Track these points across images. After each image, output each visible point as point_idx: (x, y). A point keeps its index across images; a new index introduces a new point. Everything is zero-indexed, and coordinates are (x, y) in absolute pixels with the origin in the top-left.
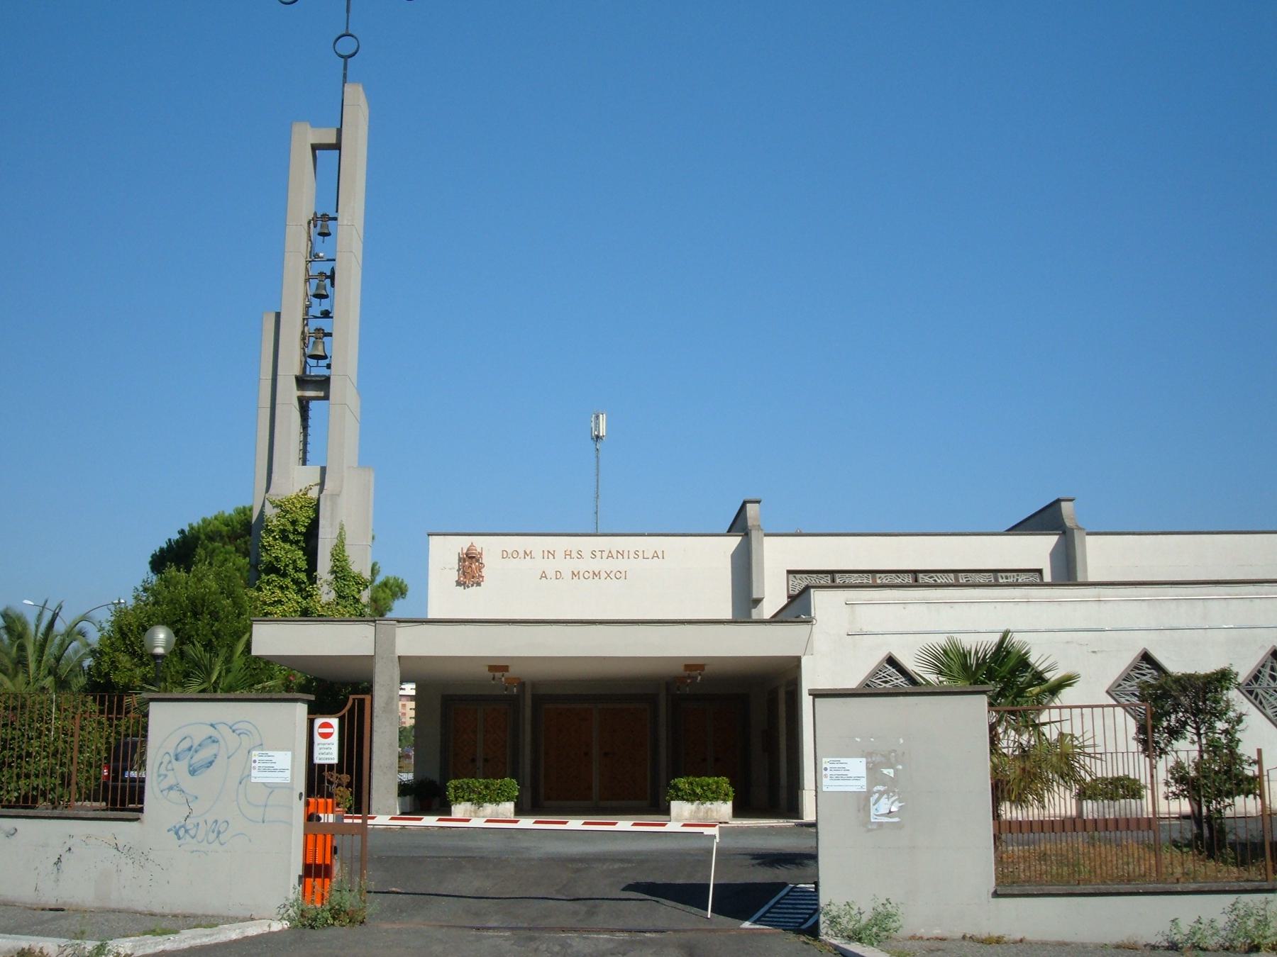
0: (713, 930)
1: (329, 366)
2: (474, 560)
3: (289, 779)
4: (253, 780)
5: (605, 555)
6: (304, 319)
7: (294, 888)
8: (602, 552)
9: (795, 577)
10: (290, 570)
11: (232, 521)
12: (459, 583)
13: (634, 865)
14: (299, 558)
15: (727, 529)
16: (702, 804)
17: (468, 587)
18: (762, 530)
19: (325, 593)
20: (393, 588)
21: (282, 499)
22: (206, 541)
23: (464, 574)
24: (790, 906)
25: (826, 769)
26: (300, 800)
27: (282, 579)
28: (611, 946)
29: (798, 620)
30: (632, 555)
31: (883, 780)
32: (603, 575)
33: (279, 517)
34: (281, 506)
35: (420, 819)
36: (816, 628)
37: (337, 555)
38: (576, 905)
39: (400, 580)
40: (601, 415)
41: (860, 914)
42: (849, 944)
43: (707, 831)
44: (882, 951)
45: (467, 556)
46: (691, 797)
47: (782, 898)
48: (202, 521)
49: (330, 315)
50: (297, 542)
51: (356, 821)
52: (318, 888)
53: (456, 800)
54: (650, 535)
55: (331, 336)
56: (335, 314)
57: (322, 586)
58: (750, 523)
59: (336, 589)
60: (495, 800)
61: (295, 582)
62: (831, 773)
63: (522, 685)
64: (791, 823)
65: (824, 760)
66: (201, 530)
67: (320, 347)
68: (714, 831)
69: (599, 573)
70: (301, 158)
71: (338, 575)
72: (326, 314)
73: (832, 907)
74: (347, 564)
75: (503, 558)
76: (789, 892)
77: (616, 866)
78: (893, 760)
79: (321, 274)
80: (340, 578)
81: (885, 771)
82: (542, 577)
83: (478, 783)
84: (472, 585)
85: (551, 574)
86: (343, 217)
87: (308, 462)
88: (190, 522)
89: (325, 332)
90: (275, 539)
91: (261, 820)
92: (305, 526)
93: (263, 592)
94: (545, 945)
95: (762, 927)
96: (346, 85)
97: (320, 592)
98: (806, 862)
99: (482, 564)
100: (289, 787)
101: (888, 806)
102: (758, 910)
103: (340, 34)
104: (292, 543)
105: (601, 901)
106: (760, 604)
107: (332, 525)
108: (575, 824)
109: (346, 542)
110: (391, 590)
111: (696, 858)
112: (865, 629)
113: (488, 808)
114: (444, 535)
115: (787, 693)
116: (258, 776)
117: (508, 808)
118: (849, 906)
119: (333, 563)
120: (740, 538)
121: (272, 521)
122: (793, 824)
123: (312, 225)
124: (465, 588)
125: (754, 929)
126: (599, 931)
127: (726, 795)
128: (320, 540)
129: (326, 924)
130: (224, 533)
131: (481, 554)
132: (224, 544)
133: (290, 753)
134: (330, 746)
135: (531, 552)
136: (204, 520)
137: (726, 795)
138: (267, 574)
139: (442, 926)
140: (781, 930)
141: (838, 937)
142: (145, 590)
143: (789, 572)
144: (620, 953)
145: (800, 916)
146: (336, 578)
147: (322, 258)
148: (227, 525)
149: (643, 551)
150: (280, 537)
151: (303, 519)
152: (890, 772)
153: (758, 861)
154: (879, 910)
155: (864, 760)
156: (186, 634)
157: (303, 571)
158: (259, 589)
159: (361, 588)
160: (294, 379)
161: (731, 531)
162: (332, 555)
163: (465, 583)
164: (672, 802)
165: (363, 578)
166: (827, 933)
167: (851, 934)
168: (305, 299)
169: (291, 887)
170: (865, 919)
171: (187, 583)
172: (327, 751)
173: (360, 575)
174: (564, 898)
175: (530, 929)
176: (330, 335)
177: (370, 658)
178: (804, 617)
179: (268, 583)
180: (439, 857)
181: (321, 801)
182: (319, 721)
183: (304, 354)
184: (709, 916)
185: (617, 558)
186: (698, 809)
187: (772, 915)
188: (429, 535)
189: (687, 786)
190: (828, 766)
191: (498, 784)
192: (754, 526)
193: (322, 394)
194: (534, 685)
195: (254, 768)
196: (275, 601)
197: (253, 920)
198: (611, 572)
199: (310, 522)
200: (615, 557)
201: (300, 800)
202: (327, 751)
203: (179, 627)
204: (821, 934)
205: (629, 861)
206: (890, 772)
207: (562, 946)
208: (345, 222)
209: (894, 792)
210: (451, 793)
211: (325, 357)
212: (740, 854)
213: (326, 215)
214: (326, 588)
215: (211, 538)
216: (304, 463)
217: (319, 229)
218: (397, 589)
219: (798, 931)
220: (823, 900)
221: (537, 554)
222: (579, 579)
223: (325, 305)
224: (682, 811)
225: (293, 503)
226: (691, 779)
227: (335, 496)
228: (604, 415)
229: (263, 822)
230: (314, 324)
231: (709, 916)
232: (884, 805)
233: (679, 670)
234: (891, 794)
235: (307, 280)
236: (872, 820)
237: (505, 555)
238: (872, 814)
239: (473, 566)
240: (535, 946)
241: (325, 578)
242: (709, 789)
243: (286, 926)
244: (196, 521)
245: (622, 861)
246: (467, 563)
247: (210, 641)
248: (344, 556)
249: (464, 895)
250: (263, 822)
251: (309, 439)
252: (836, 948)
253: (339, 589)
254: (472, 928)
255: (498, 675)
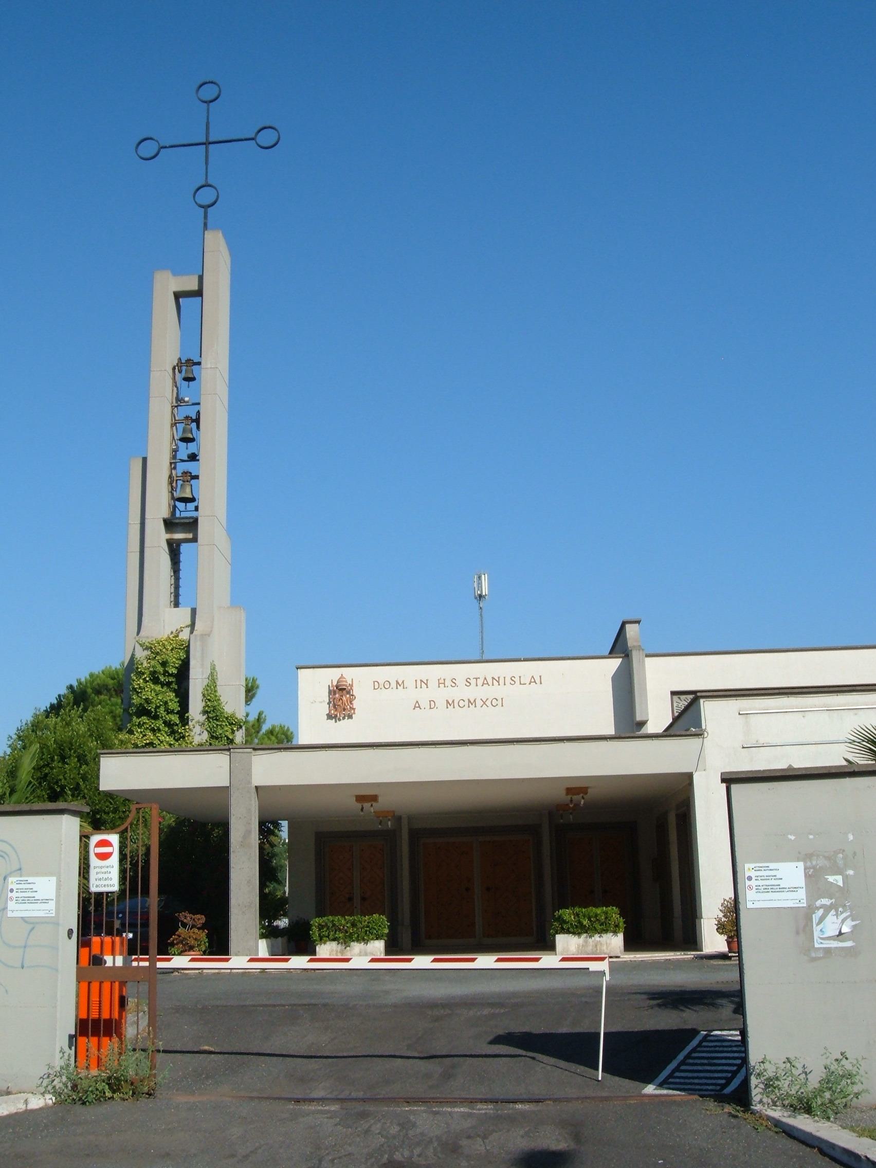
0: (606, 1099)
1: (197, 509)
2: (344, 692)
3: (54, 912)
4: (10, 914)
5: (480, 682)
6: (171, 463)
7: (62, 1051)
8: (476, 679)
9: (679, 698)
10: (162, 710)
11: (118, 675)
12: (330, 717)
13: (506, 1010)
14: (171, 700)
15: (609, 652)
16: (591, 937)
17: (340, 720)
18: (643, 650)
19: (198, 734)
20: (279, 735)
21: (152, 641)
22: (93, 695)
23: (334, 707)
24: (706, 1061)
25: (750, 878)
26: (70, 938)
27: (153, 722)
28: (467, 1124)
29: (688, 733)
30: (508, 680)
31: (829, 890)
32: (479, 703)
33: (150, 659)
34: (151, 648)
35: (410, 960)
36: (710, 741)
37: (208, 695)
38: (423, 1066)
39: (286, 728)
40: (483, 576)
41: (806, 1073)
42: (795, 1117)
43: (593, 966)
44: (844, 1128)
45: (337, 688)
46: (578, 929)
47: (694, 1050)
48: (90, 676)
49: (197, 458)
50: (168, 684)
51: (142, 964)
52: (94, 1050)
53: (321, 940)
54: (525, 660)
55: (198, 479)
56: (201, 457)
57: (194, 727)
58: (630, 643)
59: (209, 729)
60: (363, 938)
61: (167, 724)
62: (758, 883)
63: (398, 819)
64: (690, 955)
65: (747, 866)
66: (89, 685)
67: (188, 490)
68: (603, 966)
69: (475, 701)
70: (164, 307)
71: (210, 715)
72: (193, 457)
73: (767, 1065)
74: (219, 705)
75: (374, 689)
76: (701, 1042)
77: (486, 1012)
78: (840, 863)
79: (187, 418)
80: (212, 718)
81: (831, 879)
82: (415, 707)
83: (340, 920)
84: (344, 718)
85: (424, 704)
86: (207, 362)
87: (180, 605)
88: (78, 678)
89: (192, 475)
90: (145, 681)
91: (20, 965)
92: (176, 668)
93: (135, 735)
94: (379, 1125)
95: (671, 1092)
96: (206, 232)
97: (192, 734)
98: (719, 1001)
99: (353, 695)
100: (53, 922)
101: (837, 926)
102: (664, 1068)
103: (200, 185)
104: (163, 685)
105: (462, 1059)
106: (645, 726)
107: (202, 665)
108: (486, 961)
109: (218, 683)
110: (277, 737)
111: (583, 999)
112: (762, 741)
113: (355, 948)
114: (314, 668)
115: (677, 816)
116: (15, 910)
117: (378, 947)
118: (791, 1063)
119: (204, 703)
120: (621, 659)
121: (142, 664)
122: (693, 956)
123: (177, 371)
124: (336, 722)
125: (661, 1095)
126: (453, 1102)
127: (617, 926)
128: (190, 680)
129: (101, 1098)
130: (111, 687)
131: (352, 686)
132: (111, 696)
133: (55, 878)
134: (109, 870)
135: (403, 682)
136: (91, 675)
137: (617, 926)
138: (138, 717)
139: (252, 1098)
140: (696, 1097)
141: (776, 1106)
142: (19, 737)
143: (673, 693)
144: (479, 1136)
145: (720, 1075)
146: (208, 718)
147: (188, 402)
148: (113, 679)
149: (520, 677)
150: (150, 679)
151: (174, 660)
152: (837, 879)
153: (655, 1002)
154: (832, 1068)
155: (801, 865)
156: (53, 778)
157: (174, 713)
158: (131, 732)
159: (235, 729)
160: (162, 521)
161: (613, 653)
162: (204, 695)
163: (336, 716)
164: (557, 936)
165: (237, 718)
166: (761, 1102)
167: (795, 1102)
168: (171, 444)
169: (58, 1050)
170: (814, 1082)
171: (55, 728)
172: (105, 876)
173: (233, 716)
174: (416, 1055)
175: (364, 1100)
176: (197, 477)
177: (225, 790)
178: (694, 730)
179: (140, 726)
180: (274, 1006)
181: (108, 939)
182: (95, 839)
183: (173, 498)
184: (600, 1079)
185: (493, 685)
186: (586, 942)
187: (682, 1074)
188: (297, 668)
189: (572, 917)
190: (753, 874)
191: (365, 920)
192: (634, 647)
193: (190, 536)
194: (410, 818)
195: (11, 899)
196: (146, 744)
197: (8, 1093)
198: (487, 699)
199: (180, 662)
200: (490, 683)
201: (70, 938)
202: (105, 876)
203: (47, 771)
204: (754, 1103)
205: (501, 1005)
206: (837, 879)
207: (402, 1126)
208: (209, 366)
209: (844, 906)
210: (315, 933)
211: (192, 500)
212: (636, 993)
213: (190, 360)
214: (198, 729)
215: (98, 692)
216: (177, 604)
217: (183, 374)
218: (283, 736)
219: (721, 1098)
220: (754, 1056)
221: (410, 683)
222: (454, 707)
223: (192, 448)
224: (567, 943)
225: (164, 645)
226: (577, 910)
227: (206, 636)
228: (486, 575)
229: (23, 967)
230: (182, 467)
231: (600, 1079)
232: (831, 925)
233: (560, 795)
234: (840, 909)
235: (174, 424)
236: (817, 945)
237: (376, 686)
238: (815, 938)
239: (344, 698)
240: (366, 1126)
241: (196, 719)
242: (597, 920)
243: (50, 1102)
244: (84, 676)
245: (492, 1005)
246: (337, 695)
247: (78, 784)
248: (216, 696)
249: (292, 1053)
250: (23, 967)
251: (181, 582)
252: (777, 1123)
253: (211, 730)
254: (289, 1100)
255: (367, 805)
